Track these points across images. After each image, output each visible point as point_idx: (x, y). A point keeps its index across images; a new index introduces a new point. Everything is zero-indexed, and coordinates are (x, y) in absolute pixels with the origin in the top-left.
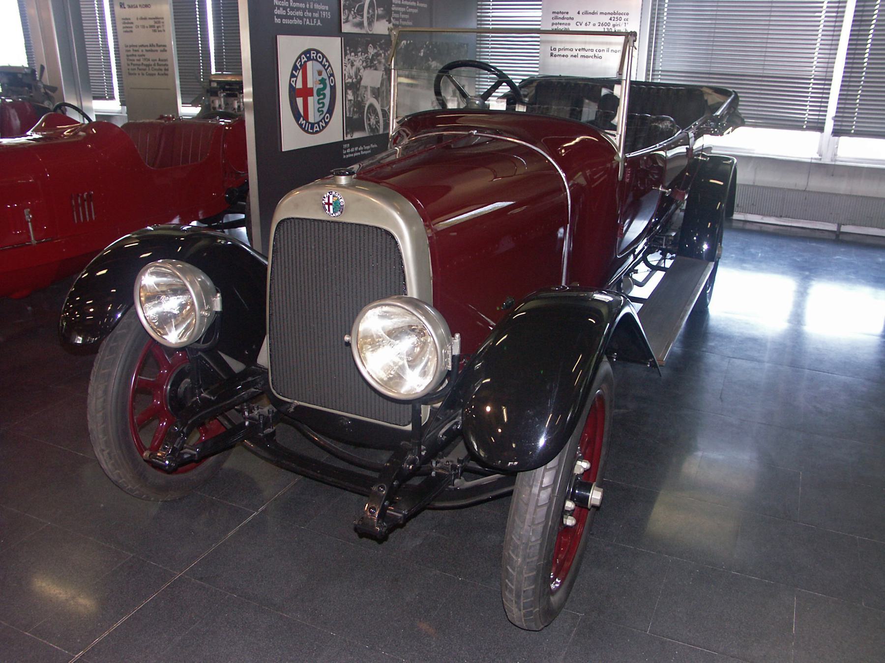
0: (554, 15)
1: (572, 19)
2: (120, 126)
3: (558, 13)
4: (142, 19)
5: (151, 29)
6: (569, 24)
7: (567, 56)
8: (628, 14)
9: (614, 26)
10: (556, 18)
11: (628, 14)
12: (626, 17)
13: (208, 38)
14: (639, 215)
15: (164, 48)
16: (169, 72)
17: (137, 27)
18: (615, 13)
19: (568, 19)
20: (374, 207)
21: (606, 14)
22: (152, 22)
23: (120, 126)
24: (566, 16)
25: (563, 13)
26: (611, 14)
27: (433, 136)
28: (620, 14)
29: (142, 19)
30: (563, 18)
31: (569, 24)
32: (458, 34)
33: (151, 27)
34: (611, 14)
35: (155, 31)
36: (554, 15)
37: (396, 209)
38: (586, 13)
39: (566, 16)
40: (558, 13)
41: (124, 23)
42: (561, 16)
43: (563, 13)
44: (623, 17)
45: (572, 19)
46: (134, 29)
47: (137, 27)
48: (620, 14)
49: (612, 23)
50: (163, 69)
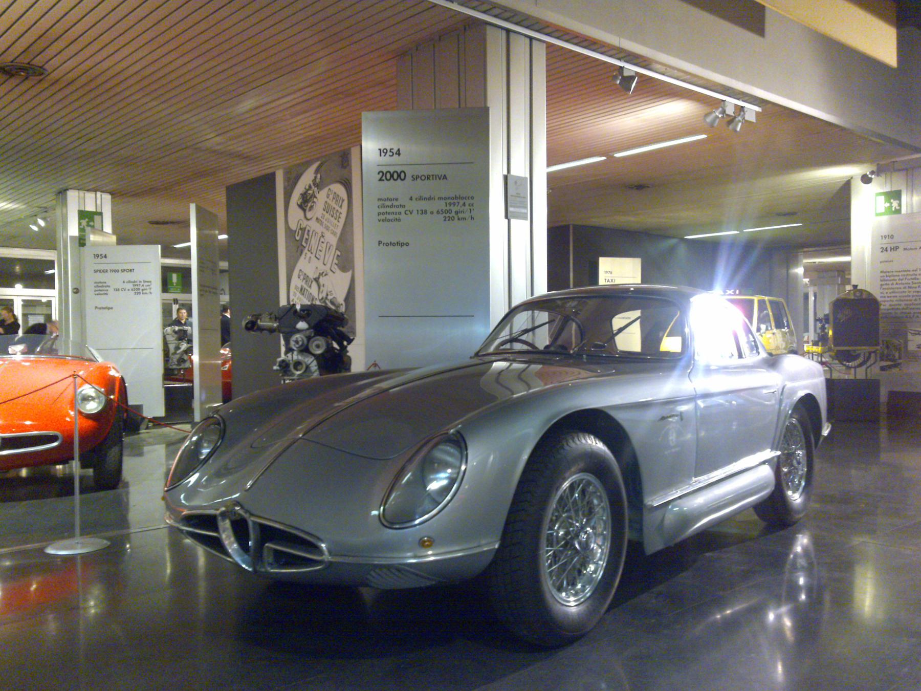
1: (404, 206)
3: (385, 200)
5: (441, 217)
8: (472, 198)
10: (383, 206)
11: (472, 198)
12: (471, 201)
13: (686, 60)
14: (842, 183)
16: (399, 169)
19: (397, 207)
24: (395, 203)
25: (391, 200)
28: (463, 198)
30: (392, 206)
32: (415, 449)
39: (395, 203)
40: (385, 200)
44: (467, 202)
46: (403, 217)
48: (463, 198)
49: (454, 209)
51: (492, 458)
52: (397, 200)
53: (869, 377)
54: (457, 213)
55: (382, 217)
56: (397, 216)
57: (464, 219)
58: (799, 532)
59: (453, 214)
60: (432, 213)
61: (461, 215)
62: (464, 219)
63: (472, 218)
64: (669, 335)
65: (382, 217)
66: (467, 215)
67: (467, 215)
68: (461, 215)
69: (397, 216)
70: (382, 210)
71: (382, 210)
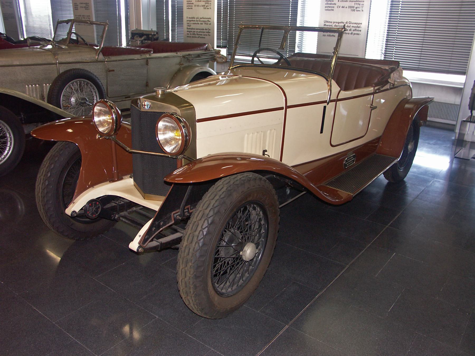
1: (335, 4)
6: (334, 7)
7: (198, 24)
9: (356, 8)
10: (327, 4)
11: (364, 1)
15: (208, 21)
17: (339, 7)
18: (357, 1)
19: (333, 4)
20: (163, 106)
21: (352, 1)
22: (84, 5)
24: (332, 3)
26: (355, 1)
27: (217, 67)
28: (359, 1)
30: (331, 4)
31: (334, 7)
33: (85, 7)
34: (355, 1)
35: (205, 8)
41: (188, 4)
43: (331, 1)
44: (361, 3)
45: (335, 4)
46: (193, 7)
47: (339, 7)
48: (359, 1)
49: (206, 5)
50: (209, 32)
51: (20, 207)
53: (176, 41)
54: (356, 8)
55: (327, 8)
56: (332, 9)
57: (359, 11)
58: (141, 30)
59: (355, 8)
60: (346, 7)
61: (358, 9)
62: (359, 11)
63: (363, 11)
64: (342, 198)
65: (327, 8)
66: (360, 9)
67: (360, 9)
68: (358, 9)
69: (332, 9)
70: (327, 6)
71: (188, 5)
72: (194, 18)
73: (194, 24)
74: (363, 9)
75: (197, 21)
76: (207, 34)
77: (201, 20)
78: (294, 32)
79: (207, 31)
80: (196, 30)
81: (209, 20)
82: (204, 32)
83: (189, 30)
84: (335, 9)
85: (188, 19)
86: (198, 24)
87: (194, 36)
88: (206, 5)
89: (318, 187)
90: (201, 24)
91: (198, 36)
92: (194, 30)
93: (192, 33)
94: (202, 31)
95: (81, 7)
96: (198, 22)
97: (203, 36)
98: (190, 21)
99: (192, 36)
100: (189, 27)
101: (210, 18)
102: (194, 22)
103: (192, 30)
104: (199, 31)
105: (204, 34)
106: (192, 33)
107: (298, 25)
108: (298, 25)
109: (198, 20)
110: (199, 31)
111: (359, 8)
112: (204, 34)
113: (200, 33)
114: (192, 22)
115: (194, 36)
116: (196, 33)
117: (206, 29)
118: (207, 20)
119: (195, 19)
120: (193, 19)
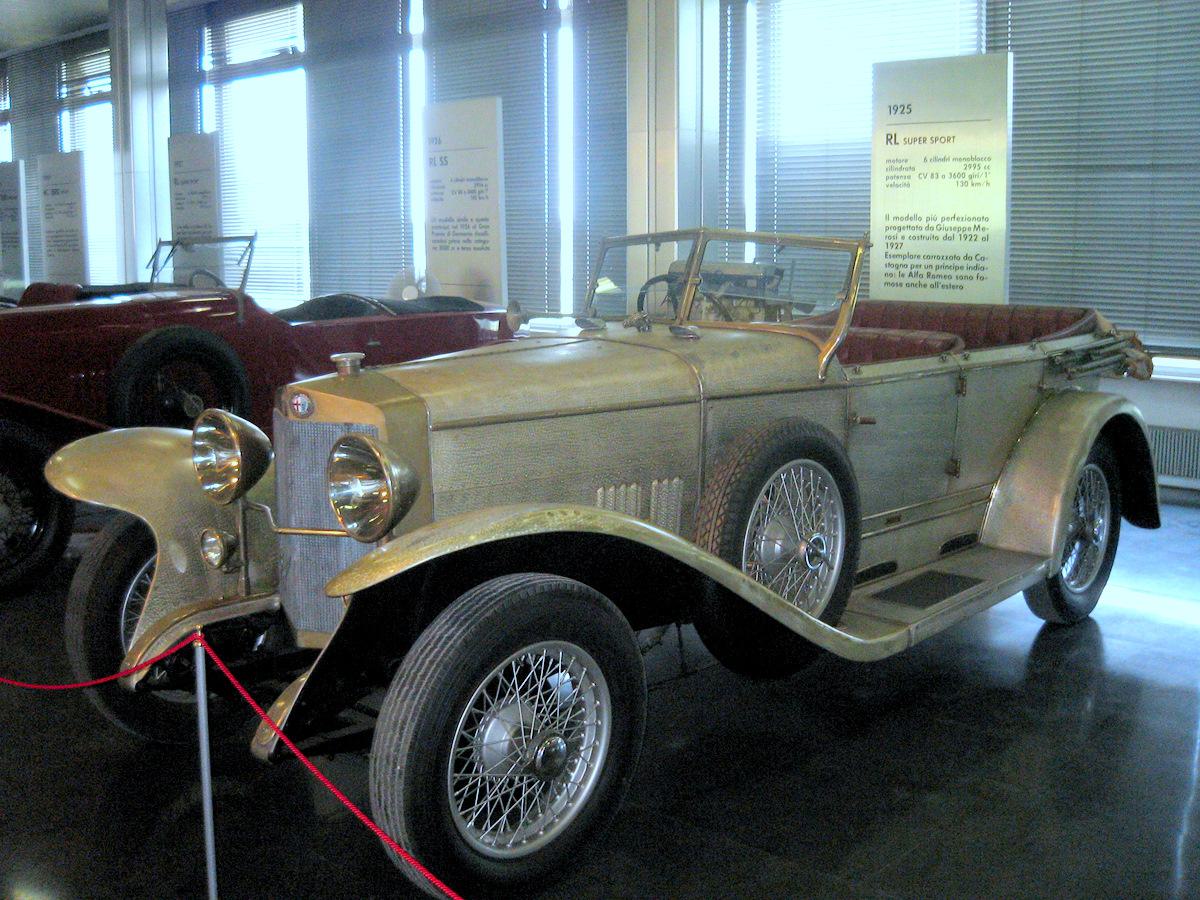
0: (888, 165)
2: (692, 625)
3: (894, 161)
4: (457, 180)
6: (909, 177)
8: (989, 159)
10: (891, 169)
12: (987, 163)
14: (221, 278)
19: (907, 169)
23: (692, 625)
24: (904, 165)
25: (900, 161)
26: (967, 159)
29: (457, 180)
31: (909, 177)
33: (470, 192)
34: (967, 159)
35: (965, 184)
36: (888, 165)
37: (1174, 841)
38: (936, 159)
39: (904, 165)
42: (898, 165)
43: (900, 161)
44: (983, 164)
46: (54, 216)
49: (969, 172)
52: (906, 161)
54: (971, 177)
55: (890, 182)
57: (979, 184)
59: (967, 178)
61: (975, 180)
62: (979, 184)
63: (487, 197)
65: (890, 182)
66: (982, 180)
67: (982, 180)
68: (975, 180)
70: (892, 174)
72: (916, 217)
73: (914, 238)
74: (990, 178)
75: (928, 228)
76: (974, 273)
77: (947, 224)
78: (739, 245)
79: (973, 263)
80: (922, 262)
81: (983, 224)
82: (956, 268)
83: (894, 261)
84: (914, 180)
85: (891, 223)
86: (937, 238)
87: (915, 280)
88: (969, 172)
89: (231, 670)
90: (946, 238)
91: (933, 281)
92: (915, 262)
93: (906, 271)
94: (949, 263)
95: (454, 192)
96: (935, 233)
97: (954, 282)
98: (900, 229)
99: (905, 280)
100: (893, 251)
101: (987, 219)
102: (917, 233)
103: (908, 261)
104: (934, 262)
105: (960, 273)
106: (906, 271)
107: (638, 225)
108: (638, 225)
109: (932, 224)
110: (934, 262)
111: (977, 176)
112: (960, 273)
113: (941, 272)
114: (907, 233)
115: (915, 280)
116: (922, 271)
117: (967, 257)
118: (971, 224)
119: (923, 224)
120: (914, 223)
